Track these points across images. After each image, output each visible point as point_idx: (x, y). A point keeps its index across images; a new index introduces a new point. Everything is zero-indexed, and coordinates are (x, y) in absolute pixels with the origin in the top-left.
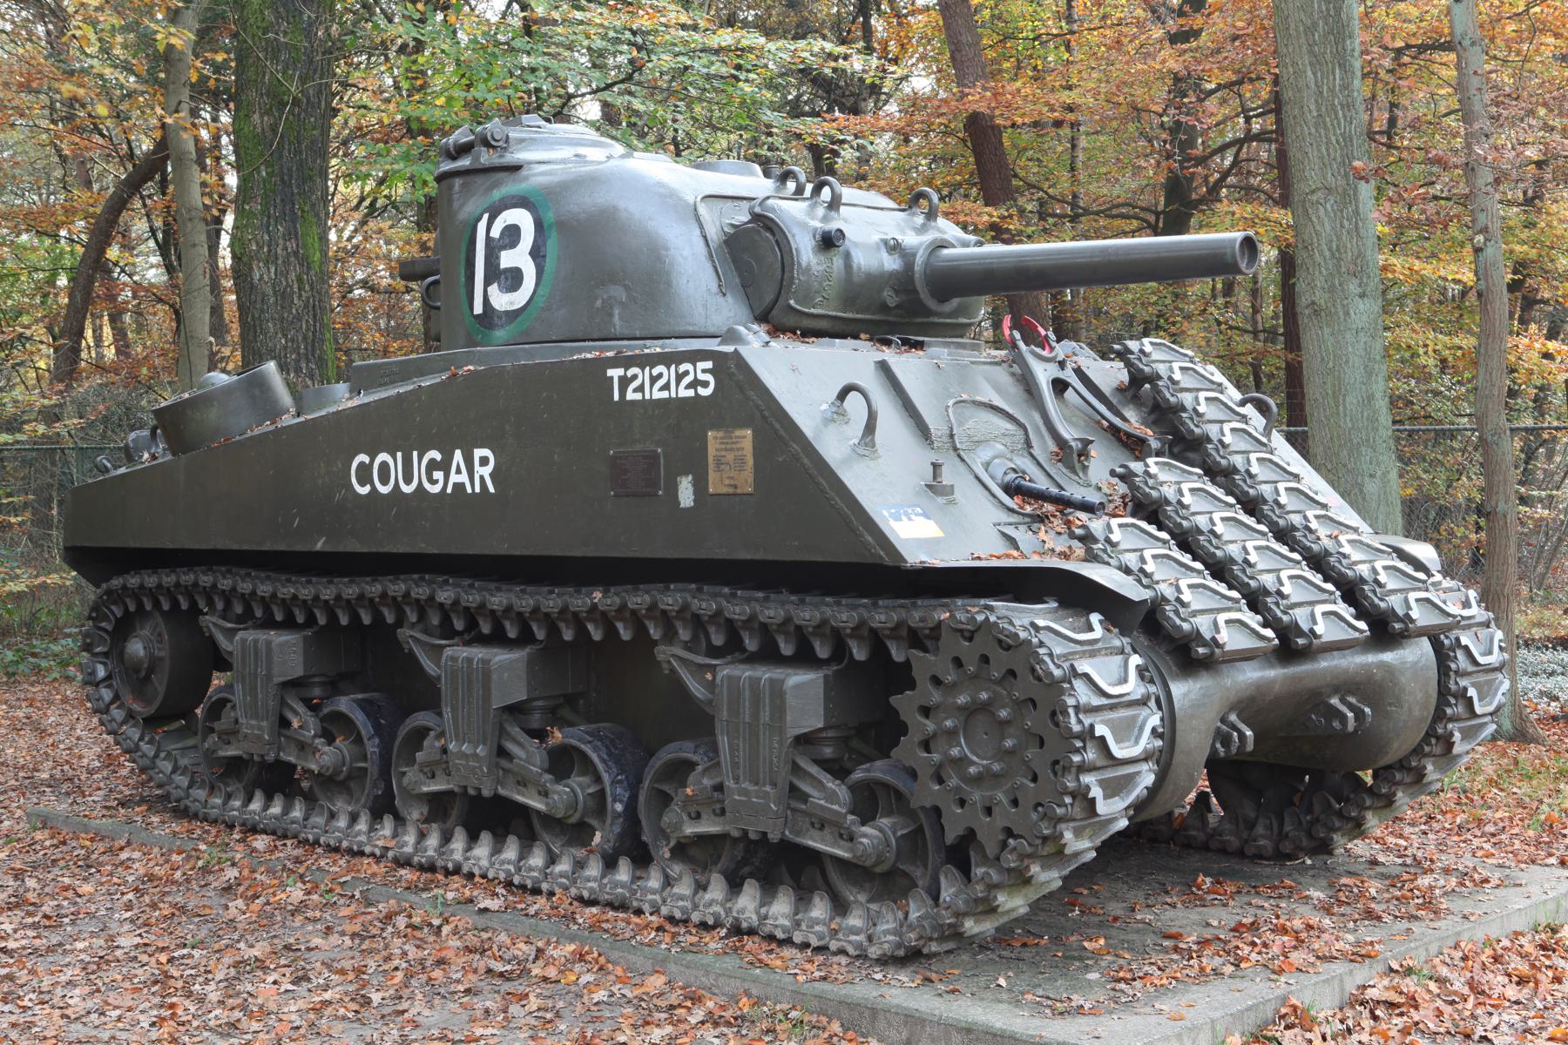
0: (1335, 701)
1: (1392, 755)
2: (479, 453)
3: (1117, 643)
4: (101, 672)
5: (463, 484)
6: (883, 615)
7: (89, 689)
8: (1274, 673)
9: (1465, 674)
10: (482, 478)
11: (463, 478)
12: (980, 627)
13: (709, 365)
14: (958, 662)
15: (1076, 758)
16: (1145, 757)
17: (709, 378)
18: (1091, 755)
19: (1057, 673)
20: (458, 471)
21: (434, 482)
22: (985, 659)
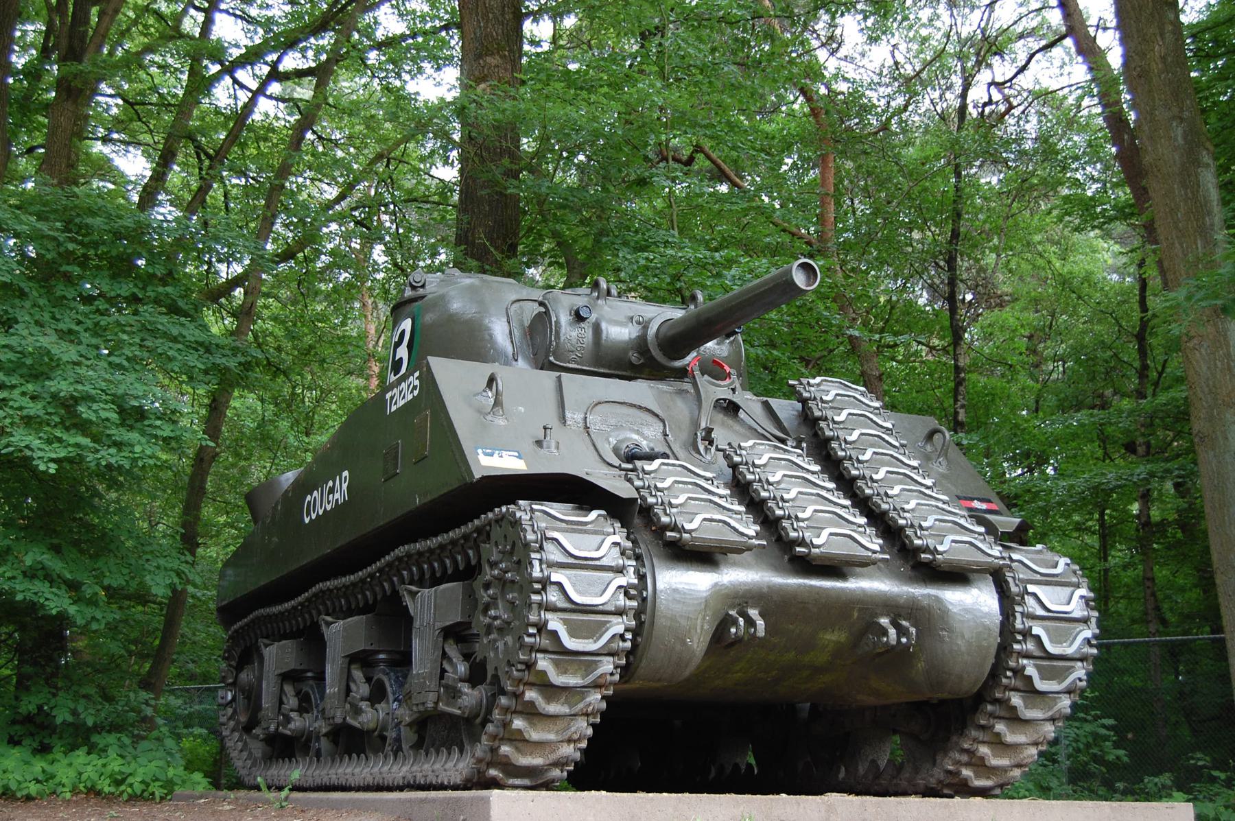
0: (884, 621)
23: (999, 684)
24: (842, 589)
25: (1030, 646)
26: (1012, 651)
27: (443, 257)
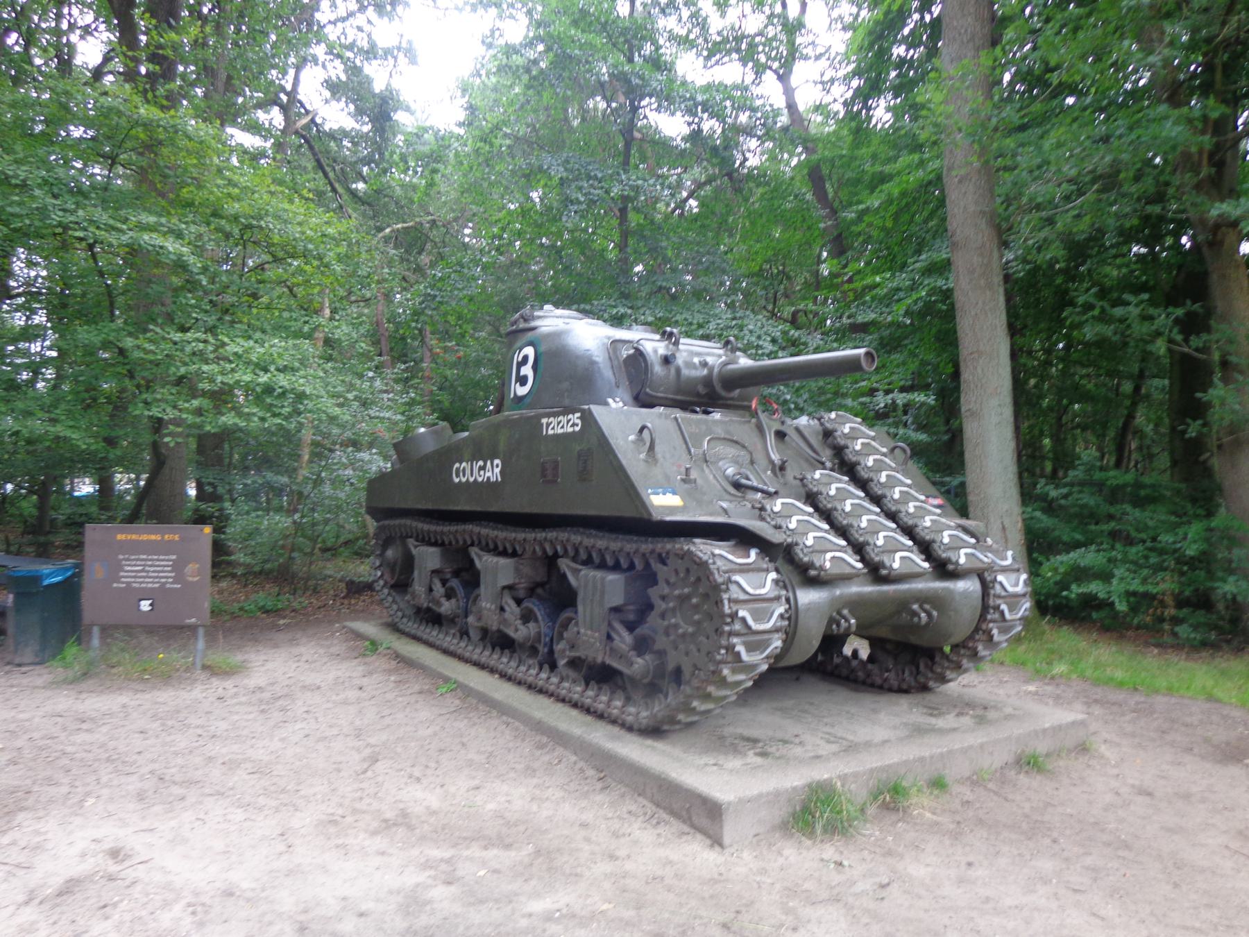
0: (915, 607)
1: (957, 638)
3: (765, 566)
4: (378, 563)
6: (646, 546)
8: (869, 589)
9: (999, 597)
14: (677, 572)
15: (727, 628)
16: (776, 630)
17: (579, 421)
18: (737, 626)
19: (720, 580)
22: (688, 571)
23: (985, 620)
24: (908, 590)
25: (737, 626)
26: (722, 633)
27: (1037, 345)
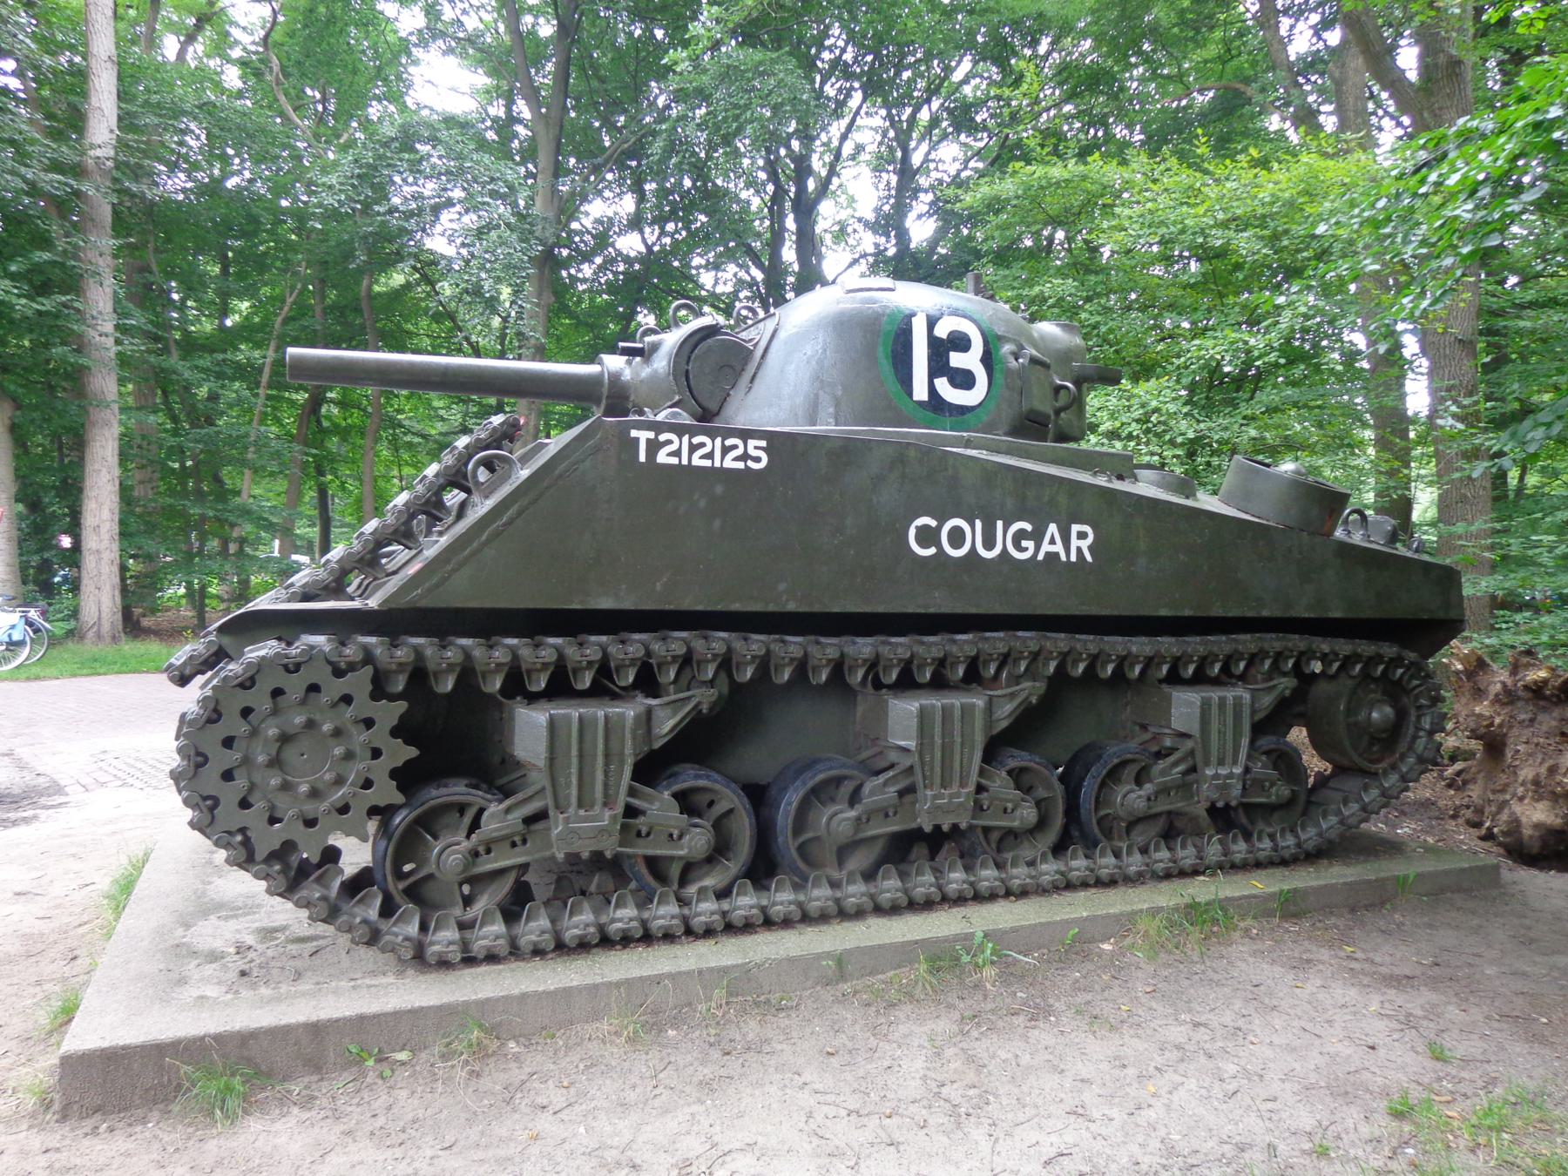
2: (1075, 528)
5: (1057, 554)
7: (312, 891)
10: (1079, 550)
11: (1059, 548)
12: (217, 702)
13: (763, 443)
20: (1052, 542)
21: (1023, 550)
